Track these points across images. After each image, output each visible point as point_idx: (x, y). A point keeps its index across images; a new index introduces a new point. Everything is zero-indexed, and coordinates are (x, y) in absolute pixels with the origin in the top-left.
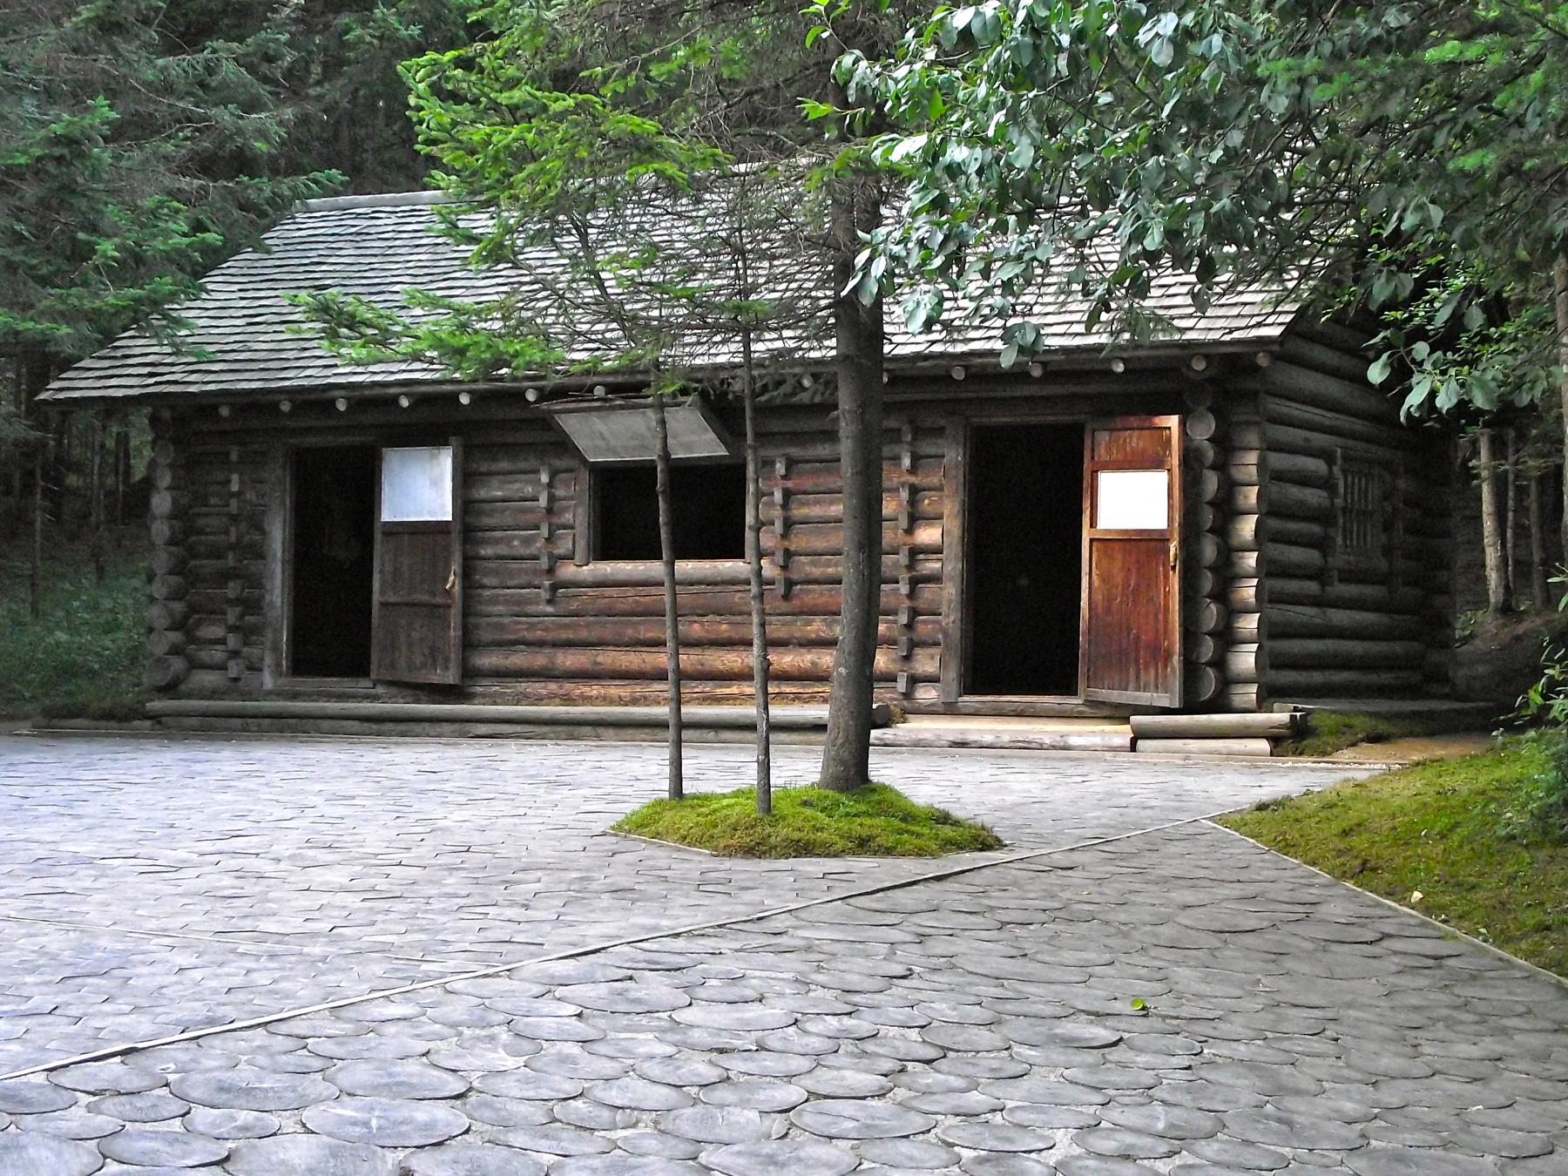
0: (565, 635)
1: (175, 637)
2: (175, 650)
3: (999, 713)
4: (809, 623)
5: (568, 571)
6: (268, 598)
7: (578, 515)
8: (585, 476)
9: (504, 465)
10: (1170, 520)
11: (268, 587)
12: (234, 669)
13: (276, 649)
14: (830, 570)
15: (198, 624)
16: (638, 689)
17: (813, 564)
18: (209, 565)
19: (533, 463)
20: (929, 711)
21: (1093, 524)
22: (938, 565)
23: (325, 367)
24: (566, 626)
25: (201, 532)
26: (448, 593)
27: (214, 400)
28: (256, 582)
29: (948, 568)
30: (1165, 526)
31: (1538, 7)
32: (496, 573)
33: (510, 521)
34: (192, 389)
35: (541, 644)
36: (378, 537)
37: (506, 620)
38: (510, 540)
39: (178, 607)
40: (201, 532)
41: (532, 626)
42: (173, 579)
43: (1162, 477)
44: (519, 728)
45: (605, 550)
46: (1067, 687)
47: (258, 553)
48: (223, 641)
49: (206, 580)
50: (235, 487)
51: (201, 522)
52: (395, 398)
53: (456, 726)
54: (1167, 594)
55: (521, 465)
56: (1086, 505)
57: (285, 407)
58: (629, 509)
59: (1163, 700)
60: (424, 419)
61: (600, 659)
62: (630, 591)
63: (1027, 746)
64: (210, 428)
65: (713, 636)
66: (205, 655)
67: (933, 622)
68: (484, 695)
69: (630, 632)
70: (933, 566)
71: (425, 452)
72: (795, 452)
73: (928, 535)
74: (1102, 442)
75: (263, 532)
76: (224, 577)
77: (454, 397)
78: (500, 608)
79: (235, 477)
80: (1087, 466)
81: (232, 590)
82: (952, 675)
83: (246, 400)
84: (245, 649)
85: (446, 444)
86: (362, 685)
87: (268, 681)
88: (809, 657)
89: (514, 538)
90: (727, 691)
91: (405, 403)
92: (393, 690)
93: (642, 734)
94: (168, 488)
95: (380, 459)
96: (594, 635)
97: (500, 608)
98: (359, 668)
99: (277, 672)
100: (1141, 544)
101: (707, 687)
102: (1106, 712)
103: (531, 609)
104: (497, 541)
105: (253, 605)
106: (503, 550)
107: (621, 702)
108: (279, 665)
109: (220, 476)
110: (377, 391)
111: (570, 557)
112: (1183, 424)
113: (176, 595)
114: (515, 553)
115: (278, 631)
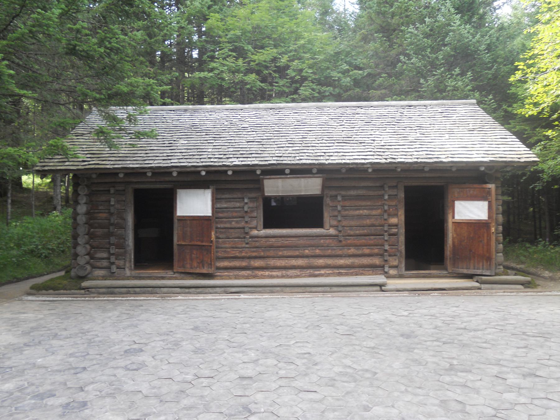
0: (254, 254)
1: (87, 257)
2: (88, 263)
4: (350, 249)
5: (255, 232)
6: (127, 243)
7: (260, 214)
10: (489, 217)
11: (127, 239)
14: (357, 232)
17: (351, 230)
18: (99, 231)
19: (240, 195)
21: (453, 217)
22: (396, 230)
23: (164, 160)
24: (254, 251)
27: (118, 171)
28: (123, 238)
34: (108, 167)
35: (243, 258)
37: (229, 250)
41: (241, 252)
44: (249, 289)
45: (266, 226)
47: (123, 227)
49: (98, 235)
50: (112, 203)
53: (223, 289)
57: (149, 174)
60: (194, 178)
61: (268, 263)
62: (280, 239)
64: (94, 183)
65: (313, 254)
66: (99, 264)
67: (395, 248)
68: (220, 276)
69: (280, 253)
70: (394, 230)
71: (202, 190)
72: (343, 193)
73: (394, 220)
74: (454, 191)
77: (199, 172)
79: (112, 199)
81: (113, 240)
83: (504, 164)
84: (116, 261)
85: (208, 188)
86: (170, 273)
87: (128, 273)
88: (351, 261)
89: (233, 221)
90: (318, 272)
92: (182, 275)
94: (85, 203)
95: (176, 194)
99: (131, 270)
101: (311, 271)
102: (455, 275)
104: (225, 223)
105: (121, 246)
108: (131, 266)
110: (193, 169)
111: (256, 228)
114: (232, 226)
115: (130, 254)
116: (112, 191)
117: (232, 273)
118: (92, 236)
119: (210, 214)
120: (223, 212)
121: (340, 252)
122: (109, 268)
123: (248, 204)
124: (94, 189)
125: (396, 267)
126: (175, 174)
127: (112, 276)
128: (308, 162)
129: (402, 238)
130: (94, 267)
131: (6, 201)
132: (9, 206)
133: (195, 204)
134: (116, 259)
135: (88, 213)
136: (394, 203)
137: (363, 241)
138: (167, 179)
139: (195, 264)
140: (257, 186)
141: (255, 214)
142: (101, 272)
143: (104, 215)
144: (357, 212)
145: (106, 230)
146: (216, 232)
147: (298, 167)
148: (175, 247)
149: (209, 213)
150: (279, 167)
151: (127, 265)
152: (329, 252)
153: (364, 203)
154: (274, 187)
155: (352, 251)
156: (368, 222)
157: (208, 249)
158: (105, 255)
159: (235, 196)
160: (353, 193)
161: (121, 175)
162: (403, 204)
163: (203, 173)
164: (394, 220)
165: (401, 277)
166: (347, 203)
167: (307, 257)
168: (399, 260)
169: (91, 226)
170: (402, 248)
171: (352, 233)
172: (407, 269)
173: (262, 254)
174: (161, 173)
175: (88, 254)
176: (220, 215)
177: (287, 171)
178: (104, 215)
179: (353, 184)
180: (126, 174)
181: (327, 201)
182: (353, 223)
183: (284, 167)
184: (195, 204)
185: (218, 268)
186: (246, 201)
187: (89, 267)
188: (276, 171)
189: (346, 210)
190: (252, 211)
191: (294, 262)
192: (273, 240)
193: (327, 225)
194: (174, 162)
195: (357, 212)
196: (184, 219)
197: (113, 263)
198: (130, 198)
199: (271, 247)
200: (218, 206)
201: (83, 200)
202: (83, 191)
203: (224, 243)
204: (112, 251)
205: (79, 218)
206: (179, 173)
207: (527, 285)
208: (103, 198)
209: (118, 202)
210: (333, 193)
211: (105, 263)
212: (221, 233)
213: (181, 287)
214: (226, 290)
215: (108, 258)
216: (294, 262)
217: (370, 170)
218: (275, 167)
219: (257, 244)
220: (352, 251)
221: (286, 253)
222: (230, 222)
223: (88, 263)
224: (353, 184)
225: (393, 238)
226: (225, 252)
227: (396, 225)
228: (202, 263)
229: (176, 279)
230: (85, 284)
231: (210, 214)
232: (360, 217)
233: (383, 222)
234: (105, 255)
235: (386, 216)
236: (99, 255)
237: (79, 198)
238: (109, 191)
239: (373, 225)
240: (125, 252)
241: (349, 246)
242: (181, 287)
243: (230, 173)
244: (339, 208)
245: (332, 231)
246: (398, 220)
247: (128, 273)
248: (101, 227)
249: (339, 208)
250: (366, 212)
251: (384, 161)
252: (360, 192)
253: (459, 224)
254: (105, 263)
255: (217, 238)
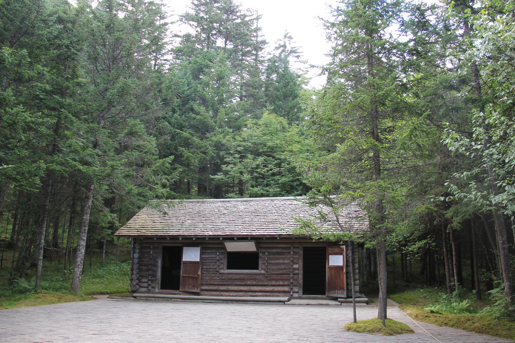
0: (221, 283)
1: (137, 281)
2: (137, 284)
3: (314, 299)
5: (222, 271)
7: (225, 262)
8: (226, 254)
9: (209, 251)
10: (343, 264)
12: (150, 288)
13: (158, 284)
15: (142, 279)
16: (236, 294)
18: (144, 268)
19: (215, 251)
20: (296, 298)
21: (328, 264)
25: (143, 261)
26: (198, 275)
28: (155, 271)
29: (300, 272)
30: (342, 265)
31: (123, 2)
32: (206, 271)
33: (210, 262)
35: (216, 285)
36: (182, 263)
38: (210, 265)
39: (138, 275)
40: (143, 261)
41: (214, 281)
42: (138, 270)
43: (341, 257)
45: (229, 268)
46: (324, 294)
47: (155, 266)
48: (148, 282)
51: (143, 259)
52: (192, 238)
54: (343, 278)
55: (213, 251)
56: (327, 261)
58: (238, 260)
59: (343, 296)
63: (321, 305)
64: (143, 242)
66: (143, 285)
70: (297, 272)
72: (269, 250)
73: (296, 266)
75: (157, 262)
76: (149, 270)
78: (207, 278)
80: (327, 254)
81: (150, 272)
82: (301, 291)
85: (198, 247)
86: (178, 292)
87: (157, 290)
91: (194, 239)
93: (242, 302)
96: (227, 283)
97: (207, 278)
98: (177, 288)
100: (340, 268)
103: (214, 278)
104: (207, 265)
105: (154, 276)
106: (208, 267)
107: (233, 296)
109: (147, 251)
111: (222, 269)
112: (346, 247)
113: (138, 273)
116: (152, 247)
117: (209, 293)
118: (140, 270)
119: (199, 260)
120: (206, 260)
121: (267, 283)
122: (147, 287)
123: (217, 255)
124: (143, 245)
125: (297, 292)
126: (180, 239)
127: (149, 292)
128: (246, 234)
129: (301, 276)
130: (140, 287)
131: (102, 252)
132: (104, 255)
133: (192, 255)
134: (152, 283)
135: (139, 258)
136: (297, 257)
137: (279, 277)
138: (176, 241)
139: (190, 287)
140: (221, 246)
141: (222, 261)
142: (144, 290)
143: (147, 259)
144: (277, 261)
145: (147, 267)
146: (202, 270)
147: (240, 236)
148: (181, 277)
149: (198, 260)
150: (231, 236)
151: (157, 286)
152: (261, 283)
153: (280, 256)
154: (231, 247)
155: (273, 283)
156: (282, 267)
157: (197, 279)
158: (146, 280)
159: (213, 251)
160: (274, 250)
161: (155, 239)
162: (302, 256)
163: (194, 239)
164: (296, 266)
165: (300, 298)
166: (272, 257)
167: (249, 285)
168: (298, 290)
169: (141, 265)
170: (301, 281)
171: (273, 272)
172: (304, 293)
173: (225, 283)
174: (174, 238)
175: (138, 279)
176: (205, 261)
177: (235, 239)
178: (147, 259)
179: (275, 246)
180: (157, 239)
181: (261, 255)
182: (274, 267)
183: (233, 236)
184: (192, 255)
185: (202, 290)
186: (218, 254)
187: (138, 286)
188: (231, 238)
189: (270, 260)
190: (221, 260)
191: (242, 288)
192: (232, 275)
193: (260, 268)
194: (181, 233)
195: (277, 261)
196: (186, 263)
197: (150, 285)
198: (160, 251)
199: (230, 279)
200: (204, 256)
201: (137, 251)
202: (137, 247)
203: (206, 276)
204: (150, 278)
205: (135, 260)
206: (183, 239)
207: (367, 303)
208: (147, 251)
209: (154, 253)
210: (264, 250)
211: (146, 285)
212: (205, 271)
213: (181, 299)
214: (204, 301)
215: (148, 282)
216: (242, 288)
217: (278, 238)
218: (229, 236)
219: (223, 278)
220: (273, 283)
221: (238, 283)
222: (210, 265)
223: (137, 284)
224: (275, 246)
225: (296, 276)
226: (207, 281)
227: (298, 269)
228: (194, 286)
229: (180, 294)
230: (135, 295)
231: (199, 260)
232: (278, 264)
233: (291, 267)
234: (146, 280)
235: (291, 264)
236: (143, 280)
237: (136, 250)
238: (150, 247)
239: (285, 269)
240: (156, 279)
241: (271, 280)
242: (181, 299)
243: (207, 239)
244: (266, 259)
245: (263, 272)
246: (298, 266)
247: (157, 290)
248: (145, 265)
249: (266, 259)
250: (281, 261)
251: (285, 233)
252: (278, 250)
253: (331, 268)
254: (146, 285)
255: (202, 273)
